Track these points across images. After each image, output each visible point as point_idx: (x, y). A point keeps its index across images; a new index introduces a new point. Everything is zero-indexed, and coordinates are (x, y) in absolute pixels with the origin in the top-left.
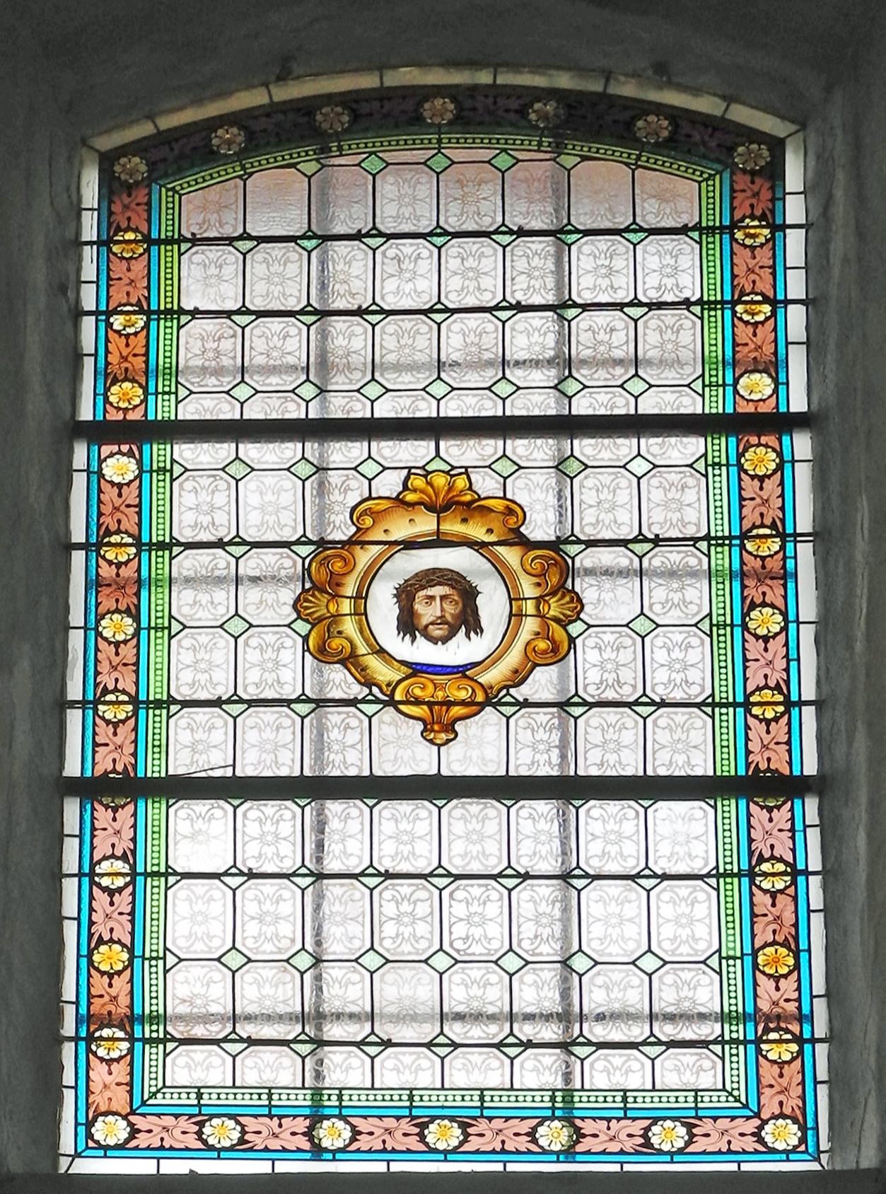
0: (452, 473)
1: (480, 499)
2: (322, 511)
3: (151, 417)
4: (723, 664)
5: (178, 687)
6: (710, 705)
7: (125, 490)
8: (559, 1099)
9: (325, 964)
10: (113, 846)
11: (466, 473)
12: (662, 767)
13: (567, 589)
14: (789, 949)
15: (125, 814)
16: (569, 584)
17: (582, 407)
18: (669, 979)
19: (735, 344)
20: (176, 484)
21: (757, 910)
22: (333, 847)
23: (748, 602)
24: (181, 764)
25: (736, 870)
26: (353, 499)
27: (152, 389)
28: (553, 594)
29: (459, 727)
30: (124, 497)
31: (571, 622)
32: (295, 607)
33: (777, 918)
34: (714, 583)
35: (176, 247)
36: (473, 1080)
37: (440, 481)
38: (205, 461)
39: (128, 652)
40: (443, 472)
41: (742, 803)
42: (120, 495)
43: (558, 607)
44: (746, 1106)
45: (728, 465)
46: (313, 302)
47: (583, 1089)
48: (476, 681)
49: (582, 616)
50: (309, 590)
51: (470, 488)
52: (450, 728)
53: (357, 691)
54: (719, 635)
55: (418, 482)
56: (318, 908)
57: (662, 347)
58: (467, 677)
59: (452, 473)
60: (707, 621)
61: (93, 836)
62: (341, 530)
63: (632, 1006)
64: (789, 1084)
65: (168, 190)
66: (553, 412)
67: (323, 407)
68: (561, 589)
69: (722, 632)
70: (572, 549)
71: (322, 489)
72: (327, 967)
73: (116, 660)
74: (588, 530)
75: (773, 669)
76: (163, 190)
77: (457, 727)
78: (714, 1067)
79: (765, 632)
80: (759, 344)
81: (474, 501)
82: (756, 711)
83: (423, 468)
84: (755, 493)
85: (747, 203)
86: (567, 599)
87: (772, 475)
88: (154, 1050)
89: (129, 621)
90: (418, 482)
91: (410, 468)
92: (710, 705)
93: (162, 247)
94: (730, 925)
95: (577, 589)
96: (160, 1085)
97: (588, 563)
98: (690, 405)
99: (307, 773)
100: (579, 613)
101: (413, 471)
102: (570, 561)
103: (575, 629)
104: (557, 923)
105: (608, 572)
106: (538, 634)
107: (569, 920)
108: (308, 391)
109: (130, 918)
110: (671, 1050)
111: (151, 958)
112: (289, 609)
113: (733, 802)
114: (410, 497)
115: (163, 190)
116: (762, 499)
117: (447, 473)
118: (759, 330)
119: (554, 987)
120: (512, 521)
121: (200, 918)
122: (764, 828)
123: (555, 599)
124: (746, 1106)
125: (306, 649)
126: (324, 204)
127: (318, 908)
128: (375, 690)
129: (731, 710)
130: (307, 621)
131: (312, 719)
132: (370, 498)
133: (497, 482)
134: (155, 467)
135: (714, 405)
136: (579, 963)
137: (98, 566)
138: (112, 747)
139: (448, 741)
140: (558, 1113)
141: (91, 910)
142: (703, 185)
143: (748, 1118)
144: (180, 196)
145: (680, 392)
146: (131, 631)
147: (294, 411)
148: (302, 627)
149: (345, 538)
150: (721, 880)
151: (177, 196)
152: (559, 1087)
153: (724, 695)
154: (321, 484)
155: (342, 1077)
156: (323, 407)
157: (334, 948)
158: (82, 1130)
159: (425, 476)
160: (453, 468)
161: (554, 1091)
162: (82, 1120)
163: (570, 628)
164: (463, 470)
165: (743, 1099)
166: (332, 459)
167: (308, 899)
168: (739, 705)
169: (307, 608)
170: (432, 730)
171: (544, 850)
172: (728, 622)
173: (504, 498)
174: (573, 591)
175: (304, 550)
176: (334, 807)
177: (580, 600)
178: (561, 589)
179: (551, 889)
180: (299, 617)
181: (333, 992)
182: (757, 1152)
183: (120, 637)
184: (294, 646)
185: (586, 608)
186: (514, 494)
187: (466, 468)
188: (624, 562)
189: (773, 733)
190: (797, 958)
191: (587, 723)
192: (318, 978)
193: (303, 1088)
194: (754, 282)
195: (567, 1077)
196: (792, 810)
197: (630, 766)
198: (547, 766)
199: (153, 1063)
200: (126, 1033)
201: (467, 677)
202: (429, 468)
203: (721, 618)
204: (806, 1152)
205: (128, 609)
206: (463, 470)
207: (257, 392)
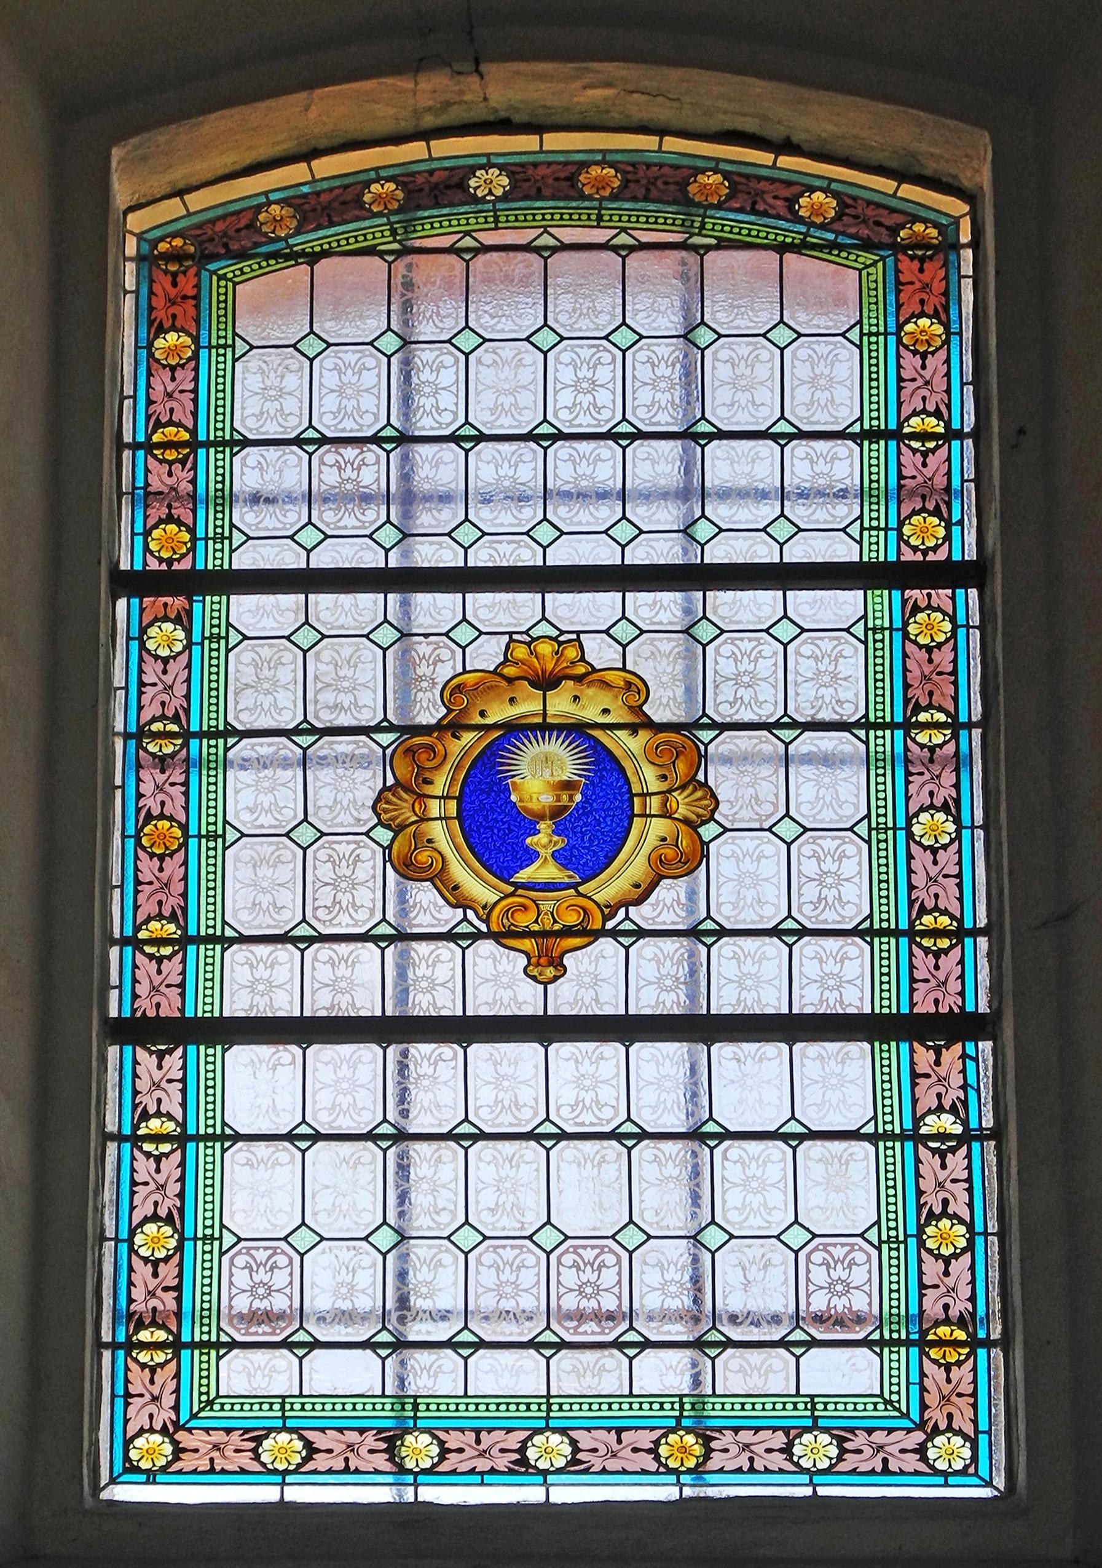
0: (562, 638)
1: (595, 670)
2: (408, 682)
3: (200, 566)
4: (879, 676)
5: (237, 712)
6: (864, 932)
7: (162, 1267)
8: (687, 1407)
9: (412, 1242)
10: (151, 1416)
11: (578, 640)
12: (809, 1002)
13: (699, 782)
14: (941, 519)
15: (173, 1061)
16: (701, 777)
17: (719, 553)
18: (803, 353)
19: (900, 476)
20: (226, 1259)
21: (926, 1280)
22: (419, 1097)
23: (925, 1211)
24: (237, 1005)
25: (897, 1131)
26: (444, 672)
27: (204, 342)
28: (683, 787)
29: (568, 960)
30: (165, 1069)
31: (704, 823)
32: (374, 808)
33: (926, 287)
34: (872, 773)
35: (221, 741)
36: (585, 1385)
37: (545, 649)
38: (268, 626)
39: (168, 1272)
40: (550, 638)
41: (905, 1047)
42: (155, 1275)
43: (687, 804)
44: (906, 1416)
45: (895, 829)
46: (390, 717)
47: (714, 1395)
48: (589, 898)
49: (716, 816)
50: (389, 789)
51: (583, 659)
52: (558, 964)
53: (448, 917)
54: (875, 641)
55: (521, 652)
56: (402, 975)
57: (824, 1082)
58: (580, 894)
59: (562, 638)
60: (857, 329)
61: (133, 1193)
62: (429, 713)
63: (761, 481)
64: (932, 377)
65: (220, 278)
66: (678, 561)
67: (406, 554)
68: (691, 783)
69: (882, 837)
70: (706, 735)
71: (406, 661)
72: (415, 1246)
73: (152, 1283)
74: (725, 709)
75: (940, 786)
76: (215, 278)
77: (565, 962)
78: (851, 456)
79: (932, 842)
80: (944, 1075)
81: (587, 674)
82: (934, 1353)
83: (526, 633)
84: (917, 468)
85: (931, 998)
86: (699, 794)
87: (960, 1254)
88: (213, 723)
89: (168, 1230)
90: (521, 652)
91: (510, 634)
92: (864, 932)
93: (212, 450)
94: (885, 987)
95: (711, 783)
96: (213, 1395)
97: (724, 749)
98: (844, 551)
99: (389, 1013)
100: (713, 811)
101: (515, 637)
102: (702, 748)
103: (708, 831)
104: (682, 986)
105: (745, 758)
106: (664, 839)
107: (697, 983)
108: (388, 535)
109: (183, 789)
110: (807, 734)
111: (218, 346)
112: (368, 814)
113: (893, 1044)
114: (510, 671)
115: (215, 278)
116: (946, 1286)
117: (555, 639)
118: (931, 459)
119: (674, 460)
120: (635, 699)
121: (261, 1291)
122: (940, 1390)
123: (685, 794)
124: (906, 1416)
125: (387, 859)
126: (407, 306)
127: (407, 378)
128: (470, 914)
129: (888, 733)
130: (388, 827)
131: (396, 652)
132: (465, 672)
133: (616, 651)
134: (200, 1235)
135: (886, 1003)
136: (713, 1237)
137: (127, 1369)
138: (160, 687)
139: (555, 979)
140: (685, 1423)
141: (135, 1076)
142: (864, 273)
143: (909, 1431)
144: (235, 284)
145: (837, 638)
146: (173, 1243)
147: (371, 558)
148: (384, 835)
149: (433, 721)
150: (872, 733)
151: (230, 284)
152: (686, 1392)
153: (894, 1356)
154: (406, 652)
155: (430, 1384)
156: (406, 554)
157: (421, 1223)
158: (139, 540)
159: (529, 644)
160: (562, 633)
161: (681, 1396)
162: (139, 528)
163: (701, 830)
164: (574, 636)
165: (904, 1410)
166: (416, 1224)
167: (394, 368)
168: (903, 933)
169: (386, 811)
170: (538, 964)
171: (664, 398)
172: (890, 824)
173: (624, 669)
174: (705, 784)
175: (385, 738)
176: (421, 1050)
177: (714, 796)
178: (691, 783)
179: (671, 543)
180: (380, 823)
181: (420, 1277)
182: (917, 1473)
183: (161, 1254)
184: (373, 858)
185: (722, 807)
186: (635, 663)
187: (578, 633)
188: (767, 748)
189: (950, 1167)
190: (948, 529)
191: (717, 651)
192: (407, 362)
193: (383, 1395)
194: (936, 896)
195: (696, 1381)
196: (969, 1156)
197: (773, 1002)
198: (673, 1003)
199: (209, 1206)
200: (181, 726)
201: (580, 894)
202: (533, 633)
203: (893, 1233)
204: (976, 1474)
205: (179, 617)
206: (574, 636)
207: (327, 537)
